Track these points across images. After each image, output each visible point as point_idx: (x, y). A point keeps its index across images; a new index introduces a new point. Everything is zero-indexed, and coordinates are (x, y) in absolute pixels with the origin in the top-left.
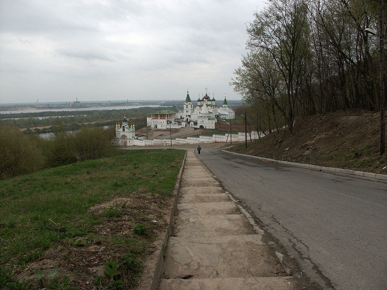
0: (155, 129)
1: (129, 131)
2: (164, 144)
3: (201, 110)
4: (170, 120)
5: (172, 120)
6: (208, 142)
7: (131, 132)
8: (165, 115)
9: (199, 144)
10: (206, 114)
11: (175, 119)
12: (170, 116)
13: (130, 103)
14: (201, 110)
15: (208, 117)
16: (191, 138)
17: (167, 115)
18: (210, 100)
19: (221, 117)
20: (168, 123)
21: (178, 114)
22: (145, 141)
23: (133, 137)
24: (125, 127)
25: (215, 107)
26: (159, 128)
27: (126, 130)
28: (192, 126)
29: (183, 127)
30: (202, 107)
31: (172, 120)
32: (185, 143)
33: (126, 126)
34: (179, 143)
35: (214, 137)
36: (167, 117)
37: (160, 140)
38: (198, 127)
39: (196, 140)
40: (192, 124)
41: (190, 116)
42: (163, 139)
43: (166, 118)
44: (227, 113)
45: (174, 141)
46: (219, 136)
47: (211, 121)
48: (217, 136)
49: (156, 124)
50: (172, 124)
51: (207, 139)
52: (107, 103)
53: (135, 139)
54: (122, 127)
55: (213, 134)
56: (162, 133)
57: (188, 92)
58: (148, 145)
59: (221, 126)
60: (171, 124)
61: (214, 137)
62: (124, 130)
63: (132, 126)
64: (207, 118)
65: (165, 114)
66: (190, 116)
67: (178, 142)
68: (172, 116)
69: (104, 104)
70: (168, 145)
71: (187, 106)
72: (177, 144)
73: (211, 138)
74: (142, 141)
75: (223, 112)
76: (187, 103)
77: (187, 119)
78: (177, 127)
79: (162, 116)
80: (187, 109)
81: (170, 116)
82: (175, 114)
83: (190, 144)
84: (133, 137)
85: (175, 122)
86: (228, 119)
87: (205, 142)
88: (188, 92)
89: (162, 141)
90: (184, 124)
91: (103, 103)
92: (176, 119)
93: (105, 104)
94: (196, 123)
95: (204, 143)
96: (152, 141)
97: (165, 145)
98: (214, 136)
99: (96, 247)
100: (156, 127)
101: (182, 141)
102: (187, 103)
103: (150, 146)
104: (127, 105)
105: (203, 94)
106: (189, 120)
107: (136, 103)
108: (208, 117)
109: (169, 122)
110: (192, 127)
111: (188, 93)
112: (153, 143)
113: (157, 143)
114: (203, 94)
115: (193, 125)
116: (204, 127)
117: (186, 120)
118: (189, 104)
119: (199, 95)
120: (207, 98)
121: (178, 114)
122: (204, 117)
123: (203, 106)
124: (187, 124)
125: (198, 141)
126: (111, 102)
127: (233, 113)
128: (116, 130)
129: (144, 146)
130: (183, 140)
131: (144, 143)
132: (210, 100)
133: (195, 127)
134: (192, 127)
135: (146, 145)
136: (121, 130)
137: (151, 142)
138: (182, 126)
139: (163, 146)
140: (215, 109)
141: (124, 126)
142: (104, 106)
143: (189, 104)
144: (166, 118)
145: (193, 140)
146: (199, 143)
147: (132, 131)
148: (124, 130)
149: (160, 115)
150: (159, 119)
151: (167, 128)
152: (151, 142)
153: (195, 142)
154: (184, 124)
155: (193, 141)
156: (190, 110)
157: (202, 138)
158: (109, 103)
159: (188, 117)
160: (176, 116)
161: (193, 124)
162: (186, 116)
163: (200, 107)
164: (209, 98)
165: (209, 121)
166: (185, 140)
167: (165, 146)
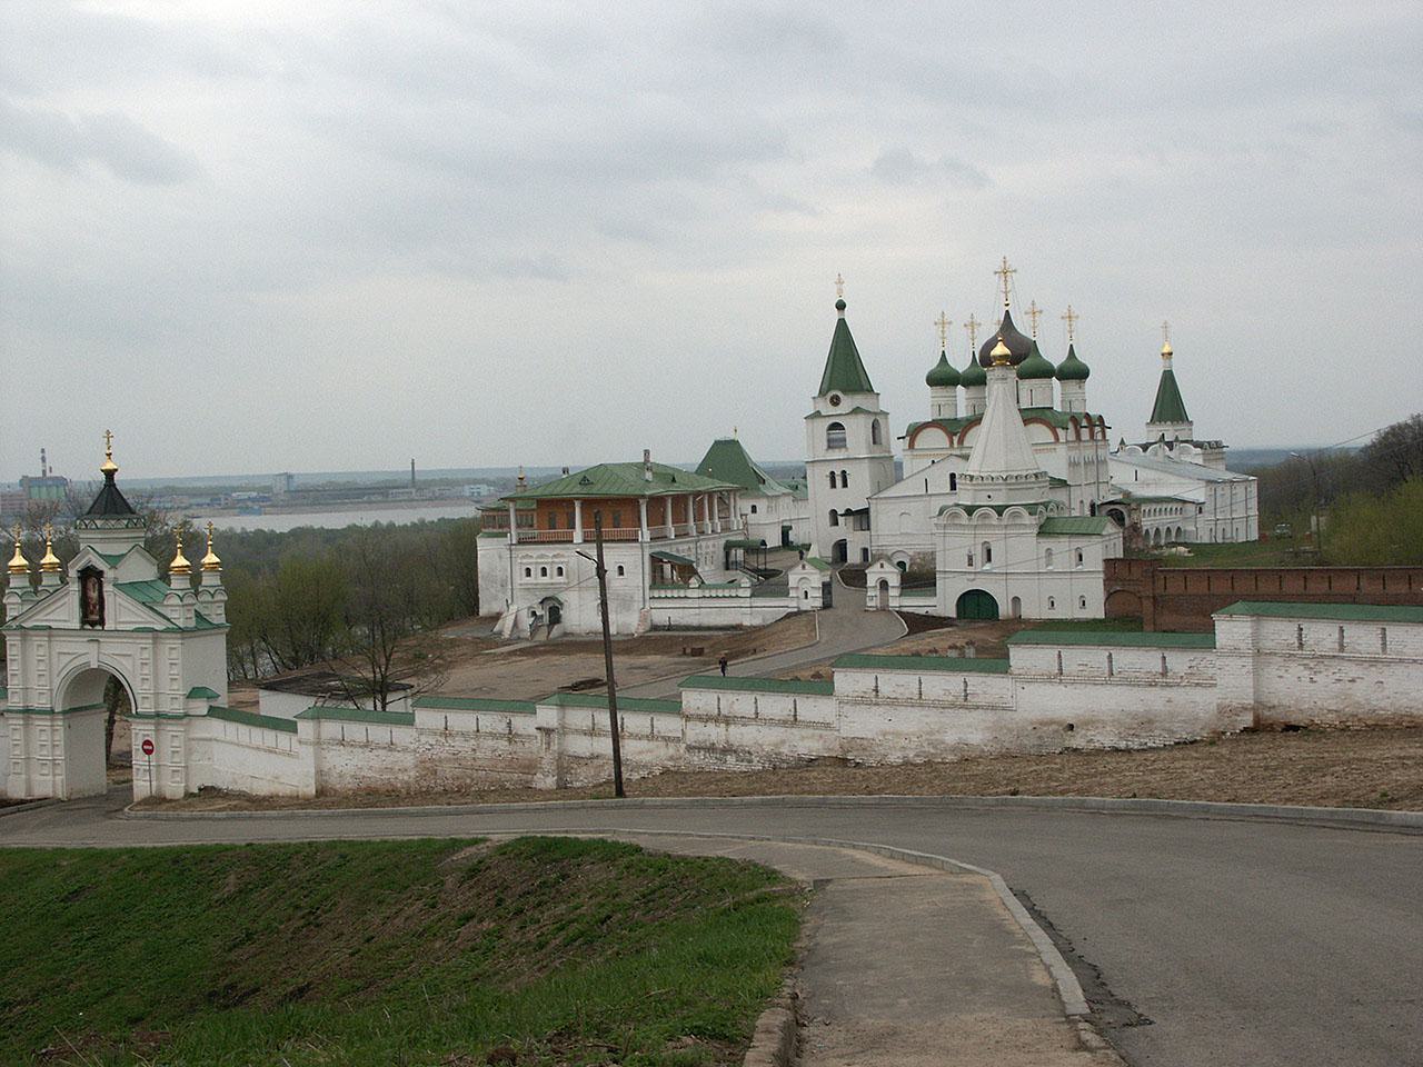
0: (541, 637)
1: (144, 618)
2: (531, 767)
3: (966, 457)
4: (683, 549)
5: (706, 551)
6: (1147, 722)
7: (182, 630)
8: (631, 502)
9: (1006, 756)
10: (1012, 482)
11: (728, 547)
12: (680, 518)
13: (428, 484)
14: (966, 457)
15: (1032, 509)
16: (896, 682)
17: (656, 502)
18: (1045, 372)
19: (1147, 523)
20: (658, 580)
21: (762, 505)
22: (318, 743)
23: (195, 693)
24: (109, 574)
25: (1085, 434)
26: (576, 629)
27: (121, 611)
28: (885, 599)
29: (799, 613)
30: (976, 438)
31: (706, 551)
32: (806, 744)
33: (114, 561)
34: (728, 750)
35: (1235, 652)
36: (657, 519)
37: (491, 721)
38: (943, 602)
39: (965, 703)
40: (884, 585)
41: (862, 517)
42: (527, 707)
43: (645, 533)
44: (1198, 493)
45: (668, 724)
46: (1322, 634)
47: (1063, 547)
48: (1279, 631)
49: (546, 587)
50: (694, 582)
51: (1130, 683)
52: (268, 489)
53: (214, 712)
54: (73, 573)
55: (1224, 602)
56: (603, 670)
57: (841, 306)
58: (349, 784)
59: (1175, 586)
60: (686, 586)
61: (1235, 652)
62: (92, 613)
63: (180, 561)
64: (1027, 519)
65: (632, 491)
66: (862, 517)
67: (715, 733)
68: (699, 517)
69: (244, 495)
70: (582, 777)
71: (836, 434)
72: (697, 759)
73: (1179, 661)
74: (284, 739)
75: (1156, 483)
76: (835, 401)
77: (841, 547)
78: (746, 609)
79: (607, 517)
80: (837, 454)
81: (680, 518)
82: (723, 499)
83: (872, 761)
84: (195, 693)
85: (732, 575)
86: (1206, 540)
87: (1089, 723)
88: (841, 306)
89: (511, 736)
90: (806, 584)
91: (235, 489)
92: (738, 545)
93: (254, 494)
94: (919, 578)
95: (1078, 741)
96: (402, 735)
97: (549, 782)
98: (1231, 629)
99: (1112, 510)
100: (555, 616)
101: (759, 724)
102: (835, 401)
103: (372, 797)
104: (411, 502)
105: (972, 325)
106: (854, 557)
107: (476, 482)
108: (1032, 509)
109: (670, 572)
110: (884, 609)
111: (848, 315)
112: (409, 760)
113: (456, 757)
114: (972, 325)
115: (893, 592)
116: (1005, 609)
117: (828, 553)
118: (857, 411)
119: (943, 323)
120: (1023, 358)
121: (762, 505)
122: (1000, 510)
123: (976, 421)
124: (839, 589)
125: (990, 716)
126: (296, 482)
127: (1240, 490)
128: (11, 613)
129: (312, 791)
130: (776, 705)
131: (307, 753)
132: (1045, 372)
133: (917, 604)
134: (884, 609)
135: (334, 782)
136: (66, 612)
137: (391, 746)
138: (791, 604)
139: (527, 790)
140: (1089, 453)
141: (101, 565)
142: (244, 508)
143: (857, 411)
144: (645, 533)
145: (919, 702)
146: (1009, 742)
147: (181, 618)
148: (92, 613)
149: (588, 503)
150: (578, 536)
151: (655, 628)
152: (391, 746)
153: (951, 738)
154: (806, 584)
155: (916, 713)
156: (866, 464)
157: (1049, 679)
158: (280, 486)
159: (845, 530)
160: (736, 523)
161: (894, 580)
162: (827, 519)
163: (951, 435)
164: (1031, 348)
165: (1047, 543)
166: (813, 708)
167: (545, 794)
